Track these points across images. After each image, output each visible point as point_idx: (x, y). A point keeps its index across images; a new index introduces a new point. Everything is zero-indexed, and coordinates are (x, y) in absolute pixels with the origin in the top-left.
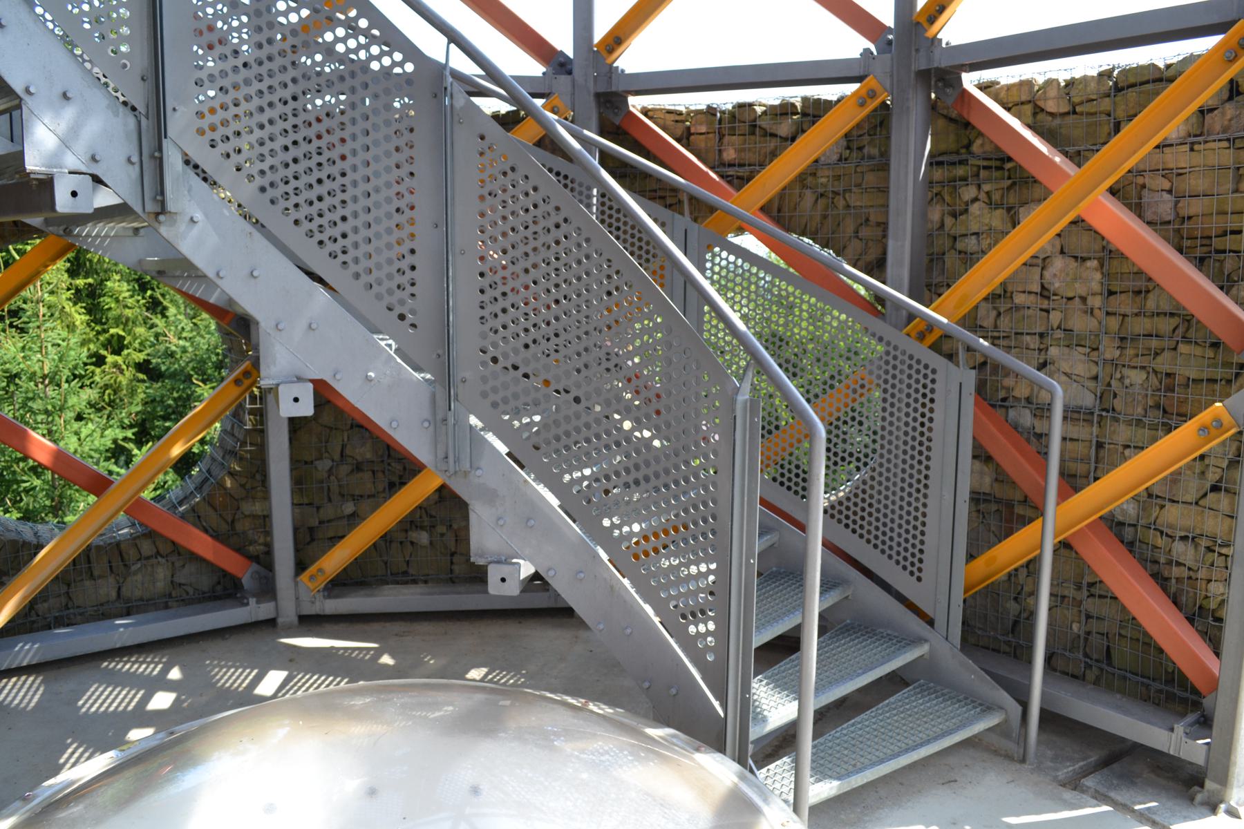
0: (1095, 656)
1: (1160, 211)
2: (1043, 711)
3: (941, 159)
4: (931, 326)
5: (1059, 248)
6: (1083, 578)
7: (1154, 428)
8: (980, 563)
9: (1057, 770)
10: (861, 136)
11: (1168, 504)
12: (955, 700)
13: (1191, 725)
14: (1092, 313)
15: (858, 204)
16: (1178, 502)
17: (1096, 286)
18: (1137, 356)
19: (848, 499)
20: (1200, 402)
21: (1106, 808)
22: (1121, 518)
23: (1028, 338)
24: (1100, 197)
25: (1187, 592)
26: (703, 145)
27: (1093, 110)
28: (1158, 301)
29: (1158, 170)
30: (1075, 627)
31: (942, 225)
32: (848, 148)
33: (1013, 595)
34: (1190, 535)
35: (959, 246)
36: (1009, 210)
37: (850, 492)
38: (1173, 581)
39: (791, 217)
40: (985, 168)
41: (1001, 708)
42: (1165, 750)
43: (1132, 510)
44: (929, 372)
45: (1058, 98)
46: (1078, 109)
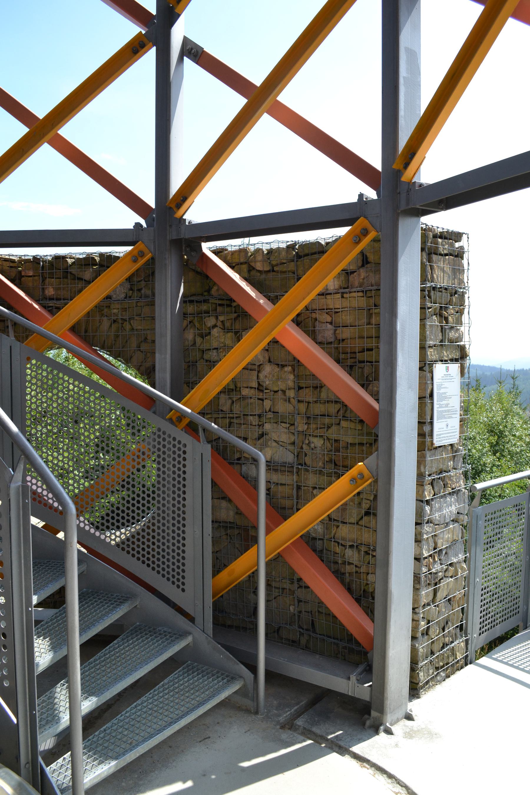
0: (305, 627)
1: (326, 335)
2: (268, 673)
3: (192, 298)
4: (182, 416)
5: (267, 358)
6: (294, 575)
7: (329, 475)
8: (224, 576)
9: (279, 715)
10: (139, 281)
11: (341, 525)
12: (210, 675)
13: (361, 674)
14: (289, 401)
15: (140, 327)
16: (346, 523)
17: (291, 384)
18: (317, 428)
19: (143, 530)
20: (355, 458)
21: (310, 742)
22: (314, 535)
23: (251, 417)
24: (287, 326)
25: (356, 581)
26: (30, 284)
27: (284, 270)
28: (327, 394)
29: (324, 309)
30: (292, 608)
31: (195, 344)
32: (131, 289)
33: (252, 590)
34: (355, 544)
35: (206, 357)
36: (236, 333)
37: (144, 525)
38: (347, 575)
39: (94, 336)
40: (220, 305)
41: (241, 677)
42: (346, 693)
43: (320, 529)
44: (181, 446)
45: (263, 261)
46: (276, 269)
